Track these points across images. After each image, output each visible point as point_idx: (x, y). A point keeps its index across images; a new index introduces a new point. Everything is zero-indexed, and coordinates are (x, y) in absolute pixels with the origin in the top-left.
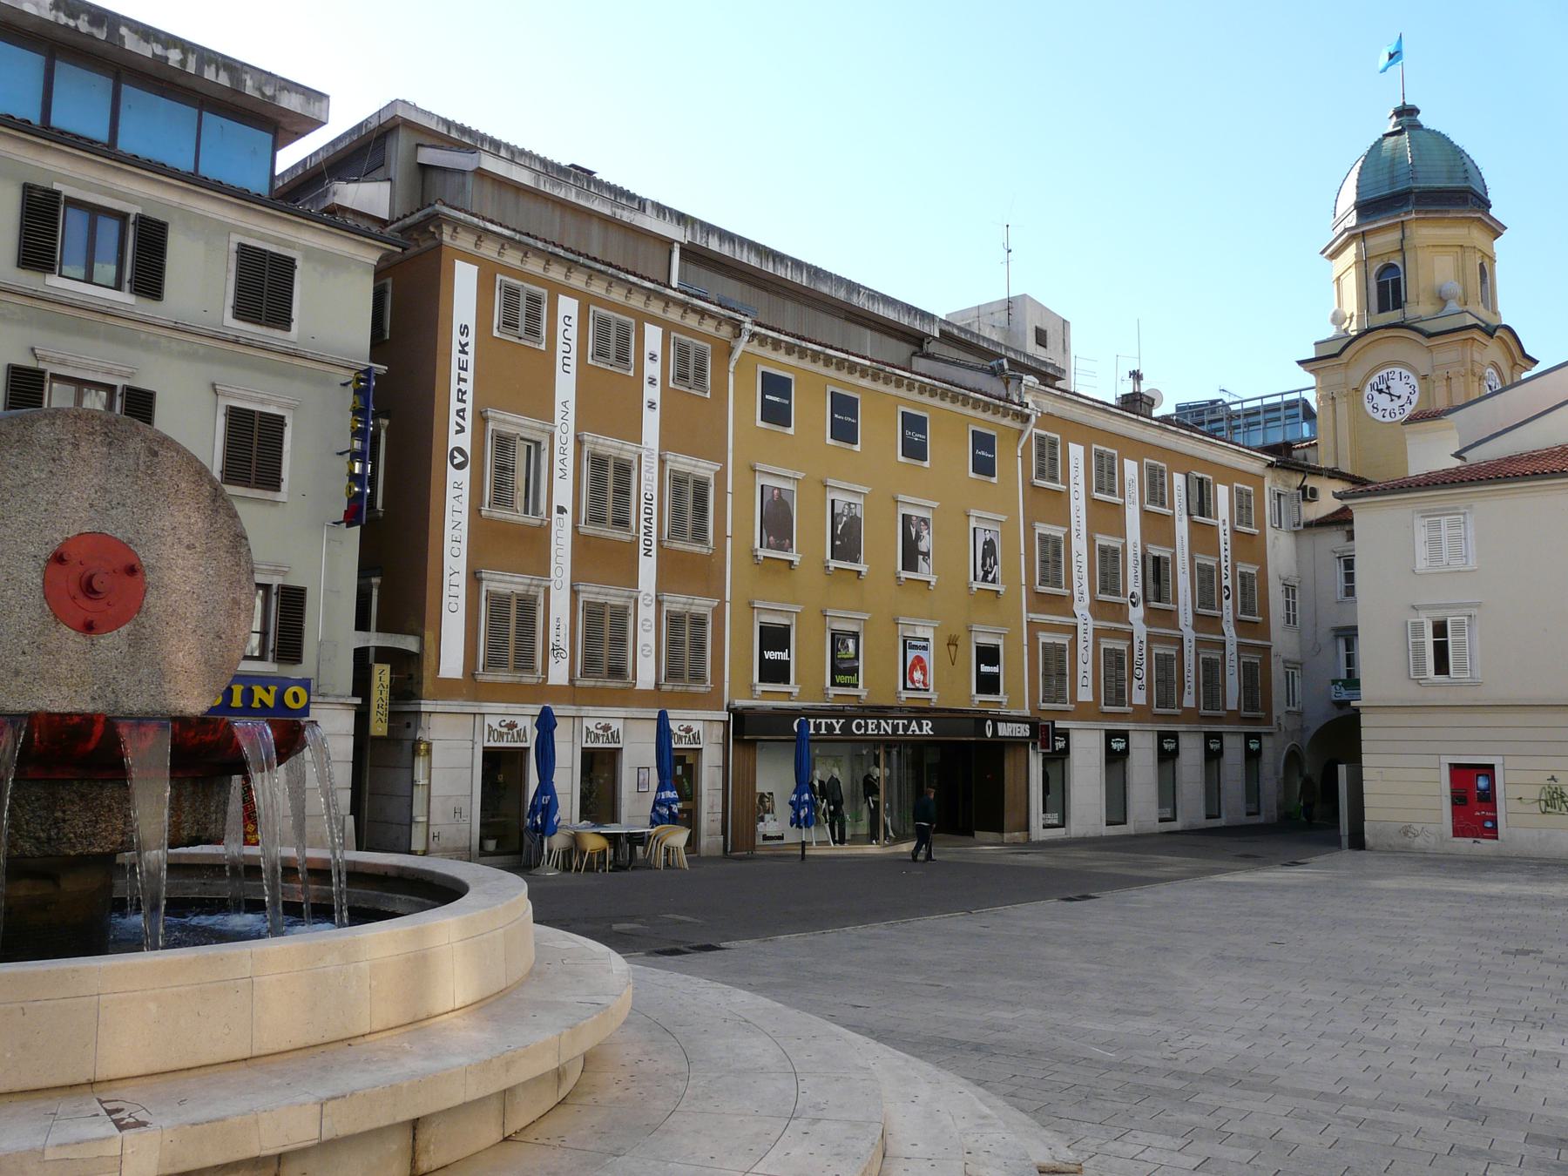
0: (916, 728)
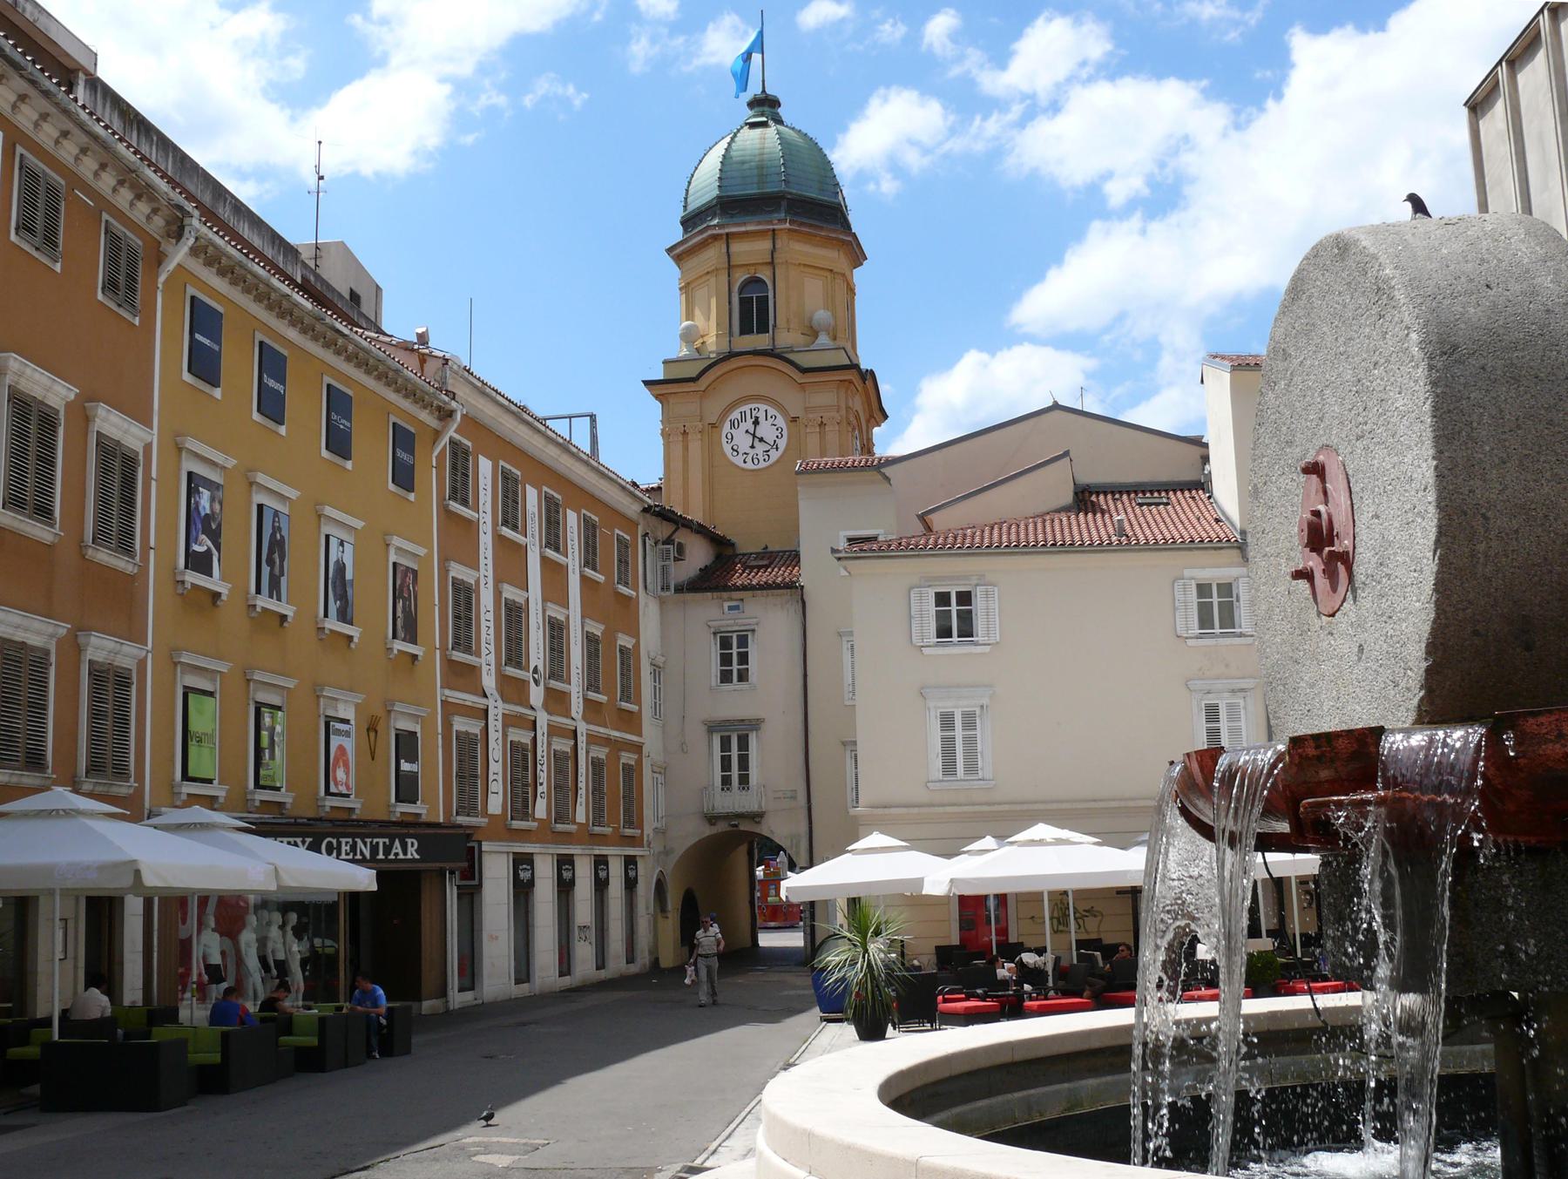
0: (400, 850)
